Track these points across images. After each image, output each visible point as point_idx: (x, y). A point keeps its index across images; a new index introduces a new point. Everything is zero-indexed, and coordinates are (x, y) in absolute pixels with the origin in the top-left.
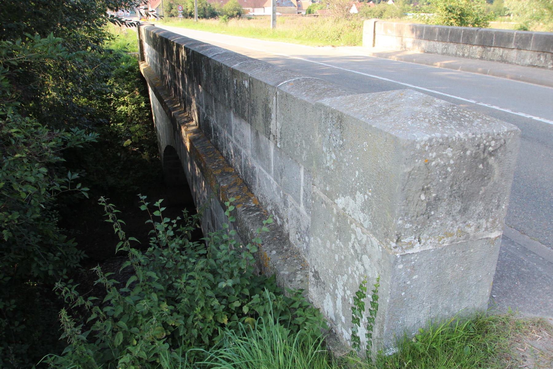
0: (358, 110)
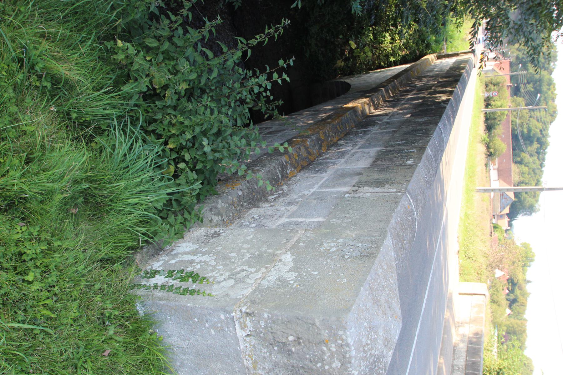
0: (380, 274)
